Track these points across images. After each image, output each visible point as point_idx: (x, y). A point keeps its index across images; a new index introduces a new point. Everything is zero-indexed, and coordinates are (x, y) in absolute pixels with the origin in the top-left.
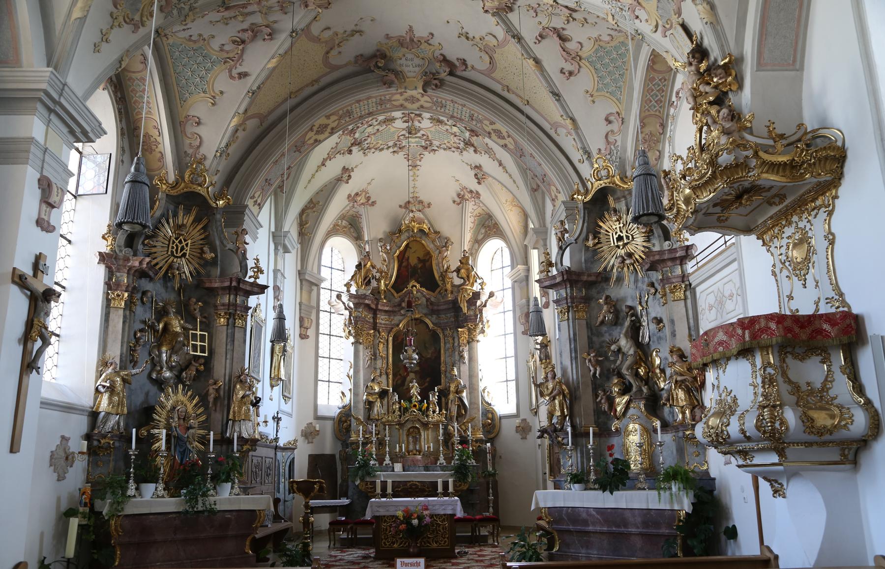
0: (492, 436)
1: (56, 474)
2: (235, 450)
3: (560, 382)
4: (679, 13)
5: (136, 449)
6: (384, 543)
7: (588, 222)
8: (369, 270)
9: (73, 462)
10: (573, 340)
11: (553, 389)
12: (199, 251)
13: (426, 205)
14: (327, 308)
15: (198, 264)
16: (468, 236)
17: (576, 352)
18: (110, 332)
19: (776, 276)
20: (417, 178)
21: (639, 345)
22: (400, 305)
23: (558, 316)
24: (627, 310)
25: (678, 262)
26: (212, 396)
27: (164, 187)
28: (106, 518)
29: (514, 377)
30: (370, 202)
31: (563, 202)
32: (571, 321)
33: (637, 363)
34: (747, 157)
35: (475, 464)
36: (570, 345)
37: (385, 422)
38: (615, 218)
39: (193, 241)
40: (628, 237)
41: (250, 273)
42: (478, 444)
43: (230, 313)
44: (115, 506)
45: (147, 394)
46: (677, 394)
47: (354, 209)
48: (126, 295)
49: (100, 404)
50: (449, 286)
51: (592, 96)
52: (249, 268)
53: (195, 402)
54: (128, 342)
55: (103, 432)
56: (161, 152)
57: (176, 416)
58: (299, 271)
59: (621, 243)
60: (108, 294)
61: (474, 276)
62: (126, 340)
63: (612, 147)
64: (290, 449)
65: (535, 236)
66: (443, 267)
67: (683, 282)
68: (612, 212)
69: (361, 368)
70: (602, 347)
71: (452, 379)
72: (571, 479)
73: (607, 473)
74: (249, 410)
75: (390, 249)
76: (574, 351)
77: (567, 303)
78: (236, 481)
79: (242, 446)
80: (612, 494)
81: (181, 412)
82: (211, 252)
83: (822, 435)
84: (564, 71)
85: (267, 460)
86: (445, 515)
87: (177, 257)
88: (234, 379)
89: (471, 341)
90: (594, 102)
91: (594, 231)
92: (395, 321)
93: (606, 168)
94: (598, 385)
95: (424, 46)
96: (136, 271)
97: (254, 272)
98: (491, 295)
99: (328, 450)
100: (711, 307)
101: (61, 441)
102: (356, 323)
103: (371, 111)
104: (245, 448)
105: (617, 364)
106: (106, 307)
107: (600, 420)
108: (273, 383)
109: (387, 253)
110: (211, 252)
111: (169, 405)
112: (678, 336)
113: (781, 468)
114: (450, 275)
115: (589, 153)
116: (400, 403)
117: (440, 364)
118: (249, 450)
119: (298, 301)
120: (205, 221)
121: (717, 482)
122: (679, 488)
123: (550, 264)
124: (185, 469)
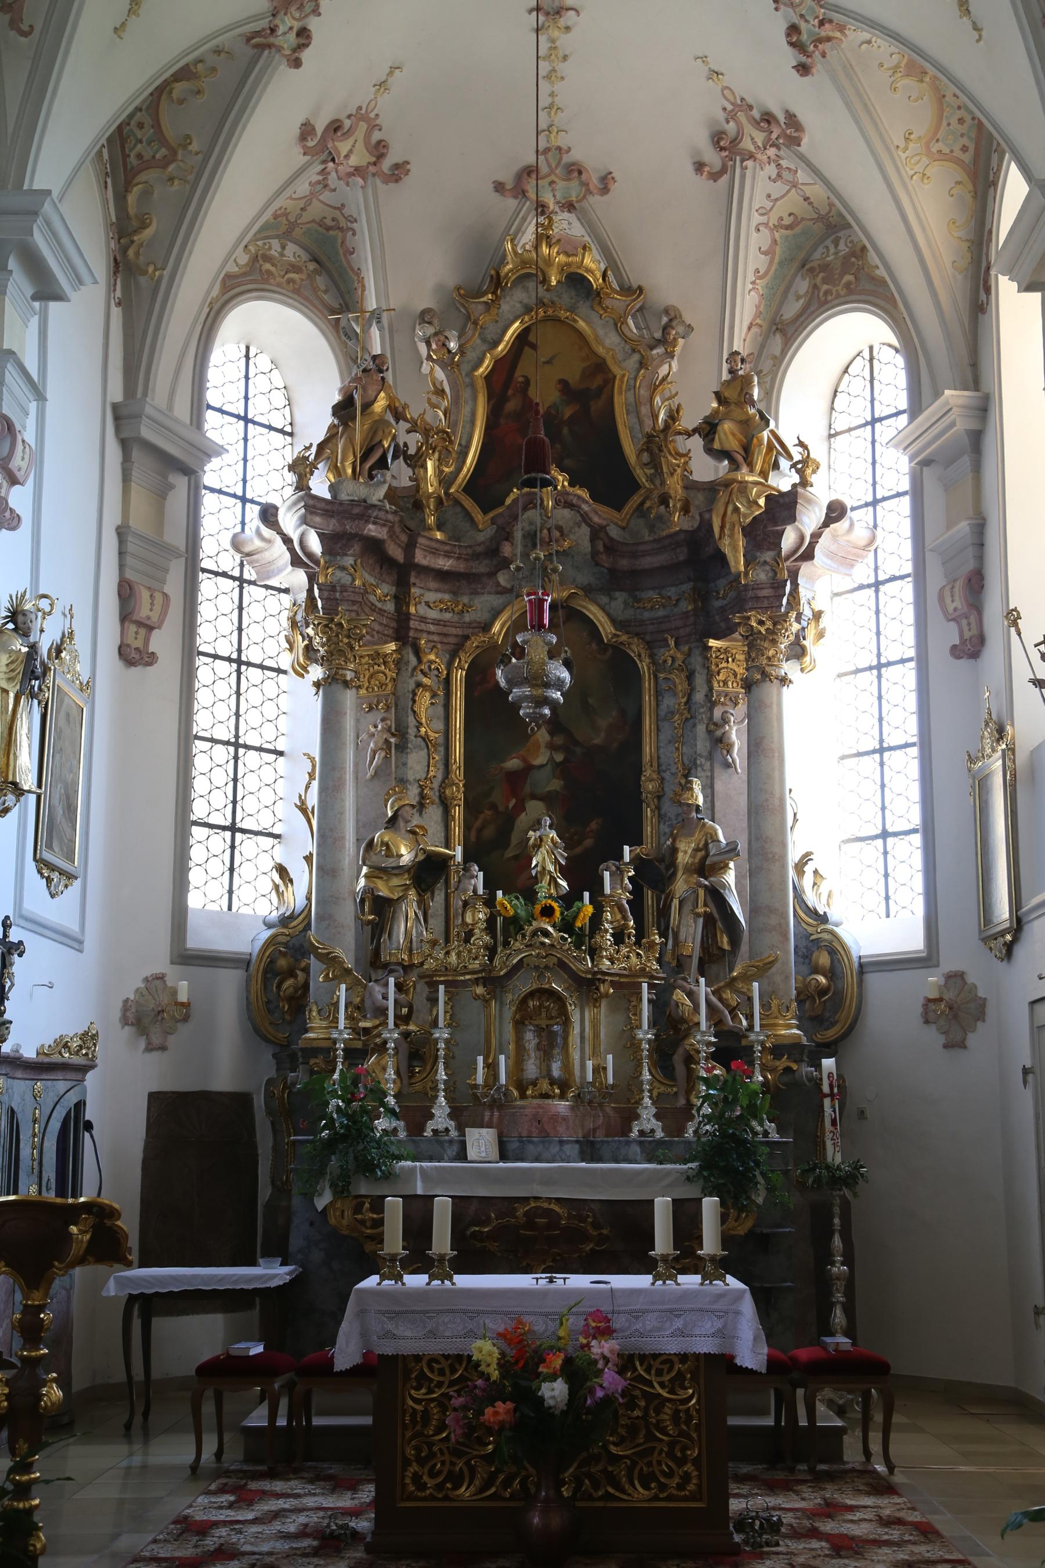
0: (831, 1034)
6: (416, 1478)
8: (379, 426)
13: (595, 182)
14: (229, 562)
20: (561, 67)
22: (492, 552)
29: (915, 818)
35: (774, 1136)
37: (435, 972)
42: (783, 1063)
47: (326, 196)
50: (674, 485)
58: (115, 407)
64: (64, 1067)
66: (655, 417)
75: (462, 350)
86: (684, 1357)
92: (478, 611)
98: (836, 512)
101: (965, 1039)
102: (331, 609)
109: (448, 363)
116: (490, 901)
117: (639, 770)
119: (112, 518)
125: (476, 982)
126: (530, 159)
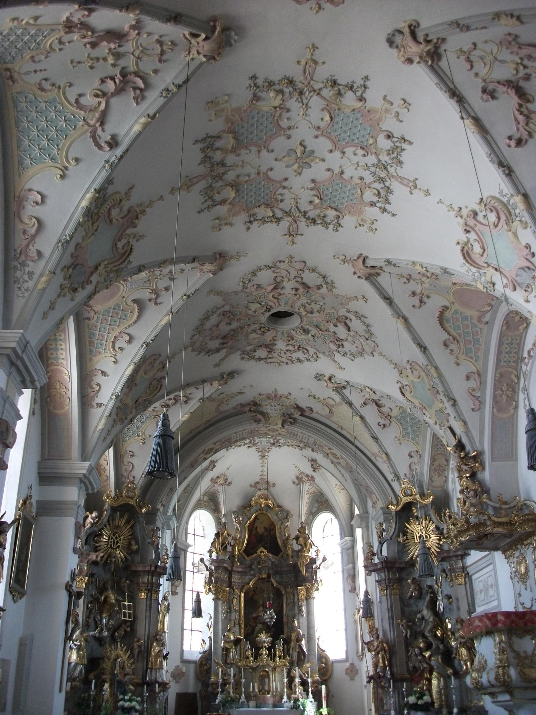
3: (382, 642)
4: (448, 421)
10: (391, 610)
11: (378, 646)
16: (305, 510)
17: (393, 619)
21: (436, 614)
22: (250, 567)
23: (380, 592)
24: (427, 589)
25: (460, 558)
26: (137, 650)
30: (227, 483)
32: (388, 596)
33: (435, 628)
34: (485, 519)
36: (389, 614)
40: (426, 537)
46: (461, 652)
47: (214, 488)
50: (290, 552)
51: (399, 440)
56: (107, 476)
61: (310, 543)
65: (360, 520)
67: (463, 572)
69: (220, 620)
71: (293, 629)
75: (242, 520)
76: (391, 618)
83: (531, 683)
84: (380, 424)
89: (309, 598)
90: (400, 444)
91: (403, 531)
94: (408, 644)
95: (283, 399)
98: (324, 559)
99: (191, 690)
100: (481, 591)
102: (216, 583)
103: (244, 437)
112: (461, 610)
113: (511, 703)
114: (291, 542)
120: (132, 523)
123: (373, 554)
125: (250, 668)
126: (258, 480)
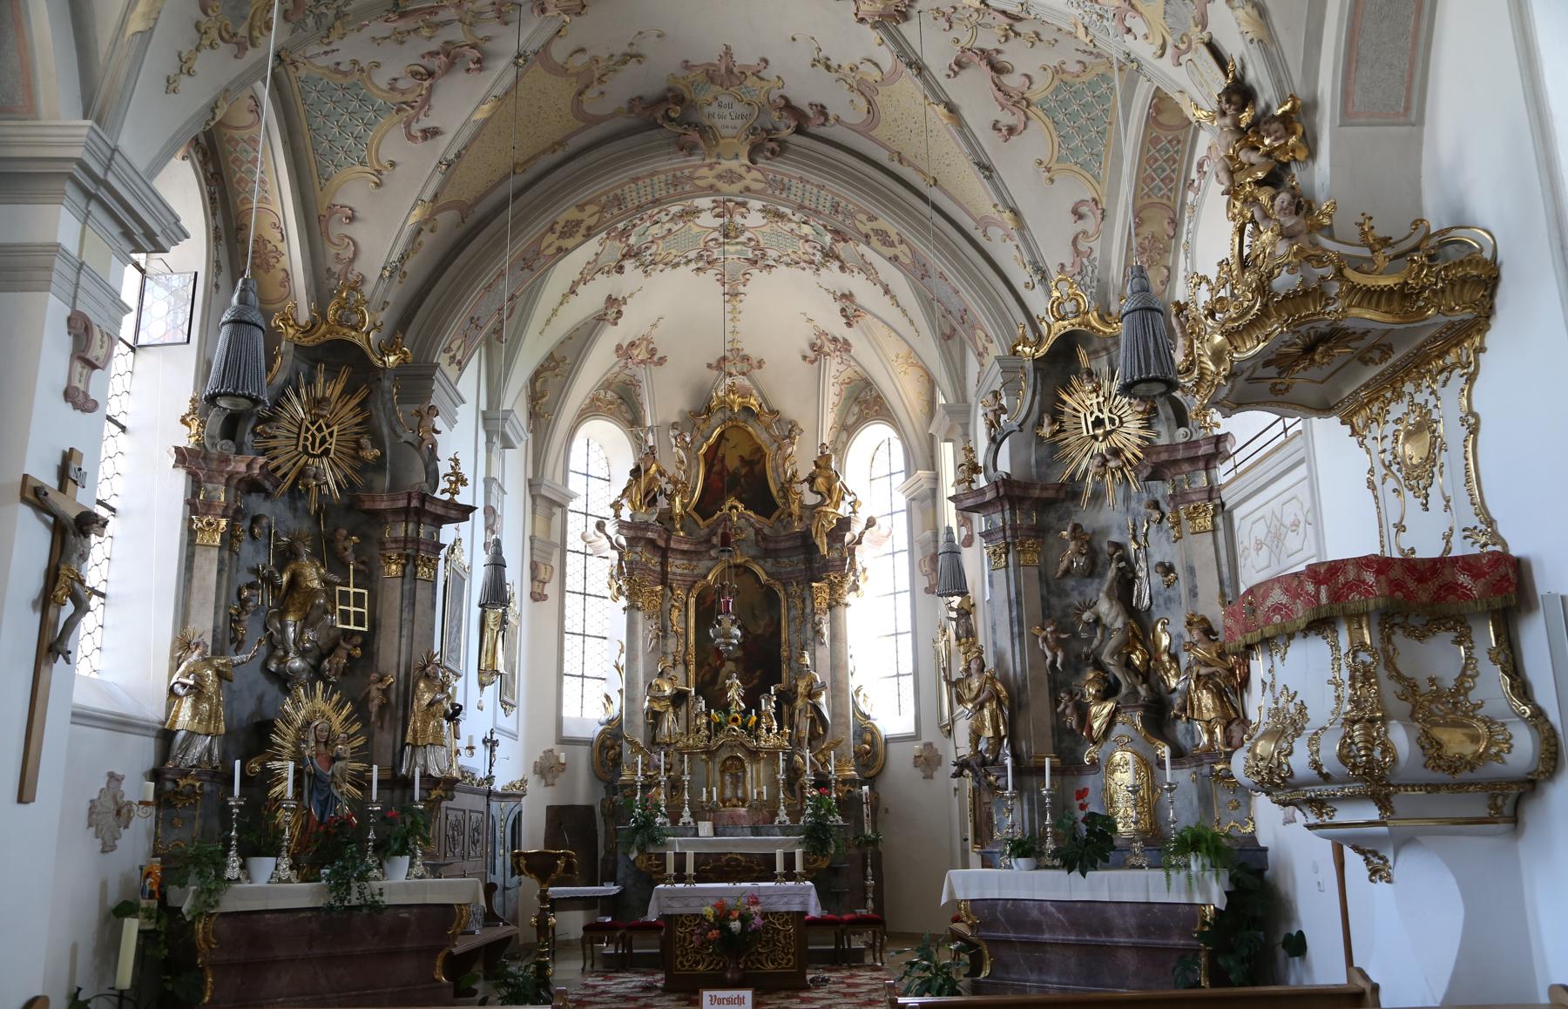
0: (872, 773)
1: (99, 841)
2: (417, 797)
3: (992, 678)
4: (1203, 23)
5: (241, 795)
6: (681, 963)
7: (1041, 394)
8: (653, 479)
9: (129, 819)
10: (1016, 602)
11: (981, 690)
12: (353, 445)
13: (755, 363)
14: (580, 546)
15: (351, 468)
16: (829, 419)
17: (1020, 623)
18: (195, 590)
19: (1374, 489)
20: (739, 316)
21: (1131, 612)
22: (708, 541)
23: (989, 561)
24: (1111, 550)
25: (1201, 464)
26: (376, 702)
27: (291, 331)
28: (188, 919)
29: (910, 669)
30: (655, 359)
31: (998, 359)
32: (1011, 569)
33: (1128, 645)
34: (1323, 278)
35: (841, 823)
36: (1011, 611)
37: (683, 748)
38: (1089, 387)
39: (342, 427)
40: (1112, 421)
41: (443, 485)
42: (847, 788)
43: (408, 556)
44: (203, 897)
45: (261, 699)
46: (1199, 699)
47: (627, 371)
48: (223, 522)
49: (176, 716)
50: (795, 508)
51: (1048, 170)
52: (441, 475)
53: (345, 712)
54: (228, 607)
55: (182, 766)
56: (285, 270)
57: (312, 737)
58: (530, 480)
59: (1100, 432)
60: (191, 521)
61: (840, 490)
62: (223, 603)
63: (1085, 260)
64: (514, 795)
65: (948, 418)
66: (786, 473)
67: (1210, 499)
68: (1085, 376)
69: (640, 653)
70: (1066, 615)
71: (801, 671)
72: (1012, 850)
73: (1075, 839)
74: (441, 726)
75: (692, 441)
76: (1017, 622)
77: (1005, 538)
78: (419, 853)
79: (428, 790)
80: (1084, 876)
81: (321, 730)
82: (373, 447)
83: (1456, 771)
84: (999, 126)
85: (474, 815)
86: (788, 913)
87: (314, 456)
88: (414, 673)
89: (834, 604)
90: (1052, 181)
91: (1053, 410)
92: (701, 570)
93: (1073, 298)
94: (1059, 683)
95: (751, 81)
96: (240, 481)
97: (451, 482)
98: (871, 523)
99: (581, 798)
100: (1259, 545)
101: (109, 782)
102: (630, 573)
103: (657, 196)
104: (434, 794)
105: (1093, 646)
106: (188, 545)
107: (1063, 745)
108: (484, 679)
109: (686, 449)
110: (373, 447)
111: (299, 717)
112: (1201, 596)
113: (1384, 829)
114: (798, 488)
115: (1044, 272)
116: (708, 714)
117: (779, 646)
118: (441, 799)
119: (528, 533)
120: (362, 393)
121: (1270, 854)
122: (1203, 866)
123: (975, 469)
124: (327, 832)
